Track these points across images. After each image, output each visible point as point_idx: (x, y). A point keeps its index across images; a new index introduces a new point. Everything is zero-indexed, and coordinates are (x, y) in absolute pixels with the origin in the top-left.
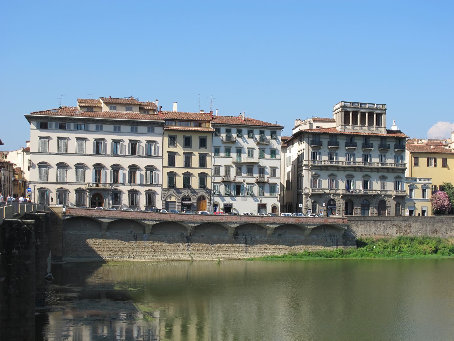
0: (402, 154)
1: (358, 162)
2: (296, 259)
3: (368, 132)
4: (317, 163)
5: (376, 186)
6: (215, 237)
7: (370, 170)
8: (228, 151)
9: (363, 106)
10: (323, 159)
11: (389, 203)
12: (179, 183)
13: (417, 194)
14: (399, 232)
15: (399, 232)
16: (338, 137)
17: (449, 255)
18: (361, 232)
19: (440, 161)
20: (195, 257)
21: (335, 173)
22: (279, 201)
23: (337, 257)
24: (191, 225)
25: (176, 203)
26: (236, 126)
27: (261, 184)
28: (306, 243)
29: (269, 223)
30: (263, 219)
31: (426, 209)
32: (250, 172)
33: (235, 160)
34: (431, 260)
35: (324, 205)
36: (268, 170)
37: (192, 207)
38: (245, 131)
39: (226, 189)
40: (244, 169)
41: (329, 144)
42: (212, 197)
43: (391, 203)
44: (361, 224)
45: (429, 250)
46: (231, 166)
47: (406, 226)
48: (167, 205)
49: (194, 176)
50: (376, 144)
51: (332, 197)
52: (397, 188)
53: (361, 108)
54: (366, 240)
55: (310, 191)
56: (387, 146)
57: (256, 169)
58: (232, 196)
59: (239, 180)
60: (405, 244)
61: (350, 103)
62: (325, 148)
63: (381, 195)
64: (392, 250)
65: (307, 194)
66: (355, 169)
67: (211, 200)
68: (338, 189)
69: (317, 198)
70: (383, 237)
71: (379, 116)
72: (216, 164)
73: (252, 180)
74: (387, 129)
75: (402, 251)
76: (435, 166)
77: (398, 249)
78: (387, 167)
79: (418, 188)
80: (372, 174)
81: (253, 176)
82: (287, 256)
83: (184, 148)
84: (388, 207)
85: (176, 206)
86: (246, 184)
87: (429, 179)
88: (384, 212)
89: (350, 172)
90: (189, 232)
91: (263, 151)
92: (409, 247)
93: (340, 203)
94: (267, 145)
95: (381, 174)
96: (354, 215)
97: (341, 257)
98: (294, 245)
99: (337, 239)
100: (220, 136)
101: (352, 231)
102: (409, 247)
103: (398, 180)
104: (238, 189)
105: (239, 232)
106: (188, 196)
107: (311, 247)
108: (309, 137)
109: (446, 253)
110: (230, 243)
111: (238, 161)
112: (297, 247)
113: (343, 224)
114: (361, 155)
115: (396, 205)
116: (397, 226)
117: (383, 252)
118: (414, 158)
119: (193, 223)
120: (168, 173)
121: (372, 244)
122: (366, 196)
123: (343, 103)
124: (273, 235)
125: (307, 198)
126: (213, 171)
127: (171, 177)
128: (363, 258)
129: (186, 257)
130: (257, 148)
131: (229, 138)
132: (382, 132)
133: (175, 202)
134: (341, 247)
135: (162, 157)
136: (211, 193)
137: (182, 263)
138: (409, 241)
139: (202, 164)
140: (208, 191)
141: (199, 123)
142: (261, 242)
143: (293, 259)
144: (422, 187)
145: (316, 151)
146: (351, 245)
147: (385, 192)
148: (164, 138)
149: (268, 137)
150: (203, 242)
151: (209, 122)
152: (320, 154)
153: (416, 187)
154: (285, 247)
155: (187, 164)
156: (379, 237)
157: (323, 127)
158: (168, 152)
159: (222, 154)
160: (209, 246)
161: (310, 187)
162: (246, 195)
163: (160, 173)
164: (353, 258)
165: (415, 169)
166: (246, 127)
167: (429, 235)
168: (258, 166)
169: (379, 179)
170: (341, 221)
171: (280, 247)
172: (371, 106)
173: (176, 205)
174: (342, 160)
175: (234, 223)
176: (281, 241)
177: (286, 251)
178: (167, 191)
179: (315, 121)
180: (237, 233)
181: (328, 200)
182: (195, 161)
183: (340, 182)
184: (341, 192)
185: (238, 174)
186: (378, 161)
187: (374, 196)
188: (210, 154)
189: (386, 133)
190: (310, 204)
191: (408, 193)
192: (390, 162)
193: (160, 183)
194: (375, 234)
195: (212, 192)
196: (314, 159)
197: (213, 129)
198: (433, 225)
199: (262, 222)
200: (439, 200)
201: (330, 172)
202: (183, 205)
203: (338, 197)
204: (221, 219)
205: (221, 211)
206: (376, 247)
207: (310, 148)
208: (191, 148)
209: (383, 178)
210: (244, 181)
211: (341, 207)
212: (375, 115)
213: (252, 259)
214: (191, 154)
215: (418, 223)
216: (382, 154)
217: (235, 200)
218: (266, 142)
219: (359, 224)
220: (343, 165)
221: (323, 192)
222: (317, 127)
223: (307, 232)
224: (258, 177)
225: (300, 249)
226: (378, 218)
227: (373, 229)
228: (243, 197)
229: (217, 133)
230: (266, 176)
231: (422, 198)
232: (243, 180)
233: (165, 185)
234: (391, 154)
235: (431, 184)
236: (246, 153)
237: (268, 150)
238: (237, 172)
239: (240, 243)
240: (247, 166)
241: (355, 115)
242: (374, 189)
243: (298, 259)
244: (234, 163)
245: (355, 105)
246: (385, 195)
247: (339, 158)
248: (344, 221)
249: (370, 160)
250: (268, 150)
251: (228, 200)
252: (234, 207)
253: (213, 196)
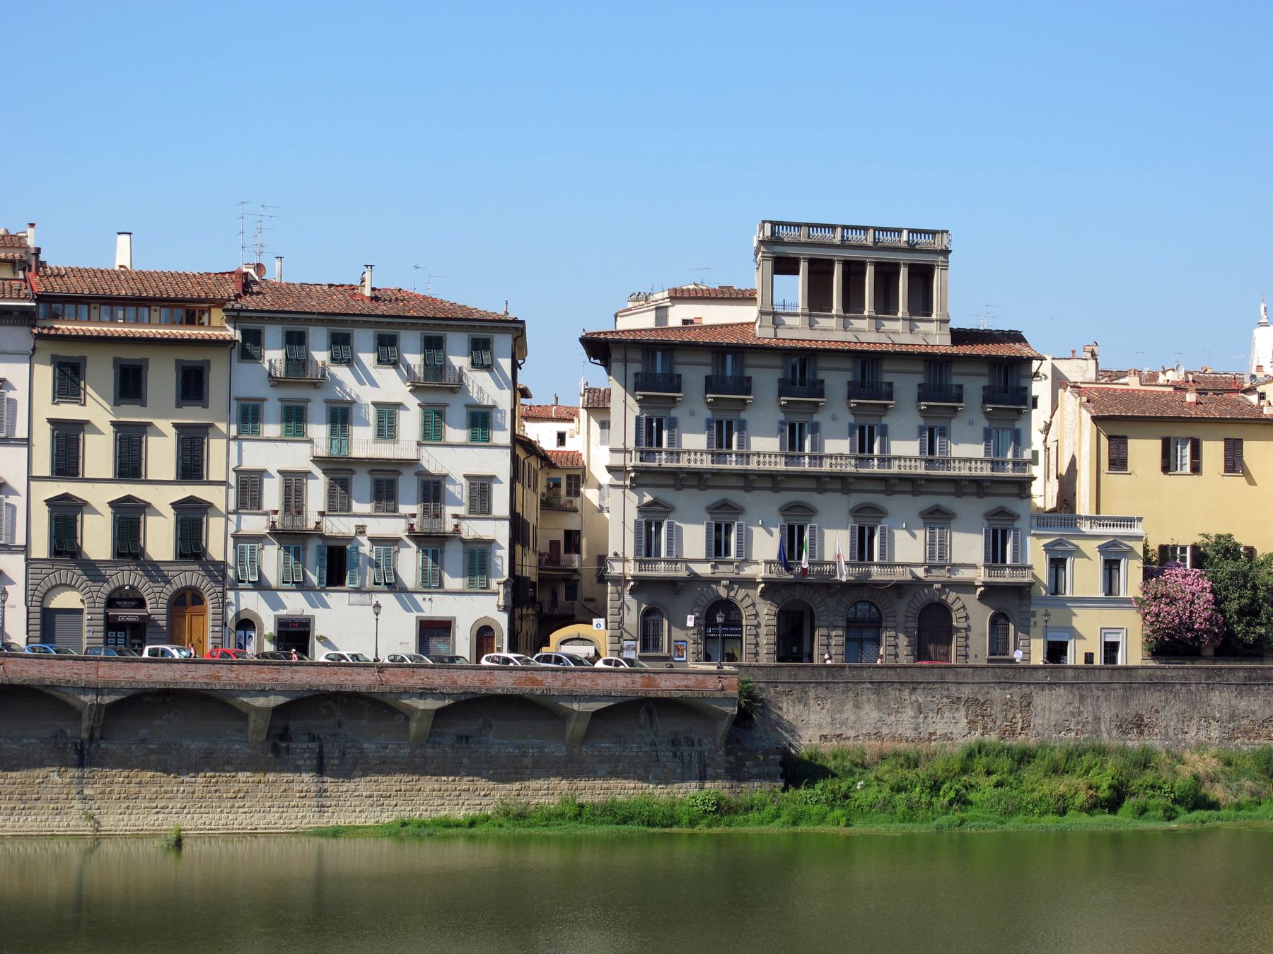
0: (1018, 425)
1: (831, 456)
2: (523, 831)
3: (872, 337)
4: (662, 461)
5: (908, 548)
6: (195, 746)
8: (295, 418)
9: (854, 237)
10: (685, 446)
11: (962, 613)
12: (97, 538)
13: (1084, 576)
14: (980, 725)
15: (980, 725)
17: (1170, 819)
18: (820, 726)
19: (1213, 451)
20: (111, 821)
21: (737, 497)
22: (505, 609)
23: (692, 823)
24: (88, 699)
25: (86, 617)
26: (326, 318)
27: (432, 543)
28: (571, 768)
29: (408, 692)
30: (386, 676)
32: (385, 495)
33: (322, 451)
34: (1094, 837)
35: (690, 623)
36: (458, 489)
37: (148, 630)
38: (363, 339)
39: (286, 564)
40: (362, 483)
41: (711, 385)
42: (231, 595)
43: (974, 617)
44: (817, 698)
45: (1081, 798)
46: (307, 474)
47: (1008, 704)
48: (47, 623)
49: (158, 514)
50: (906, 384)
51: (723, 592)
52: (995, 555)
53: (877, 246)
54: (835, 757)
55: (631, 570)
56: (885, 388)
57: (408, 485)
58: (311, 589)
59: (339, 526)
60: (989, 773)
61: (799, 225)
62: (694, 400)
63: (930, 584)
65: (620, 581)
66: (822, 482)
67: (225, 605)
68: (747, 561)
69: (660, 596)
70: (902, 746)
71: (922, 277)
72: (247, 465)
73: (392, 527)
74: (955, 324)
75: (970, 803)
76: (1196, 469)
77: (952, 794)
78: (952, 473)
79: (1084, 556)
80: (891, 503)
81: (395, 510)
82: (487, 818)
83: (116, 403)
84: (958, 630)
85: (85, 629)
86: (368, 544)
87: (1131, 520)
88: (942, 649)
89: (797, 496)
90: (86, 724)
91: (440, 414)
92: (999, 785)
93: (761, 618)
94: (453, 390)
95: (927, 502)
96: (816, 663)
97: (709, 825)
98: (522, 780)
99: (700, 754)
100: (261, 357)
101: (779, 722)
102: (999, 785)
103: (999, 525)
104: (337, 564)
105: (294, 725)
106: (132, 588)
108: (626, 361)
109: (1156, 808)
110: (255, 771)
111: (335, 453)
112: (534, 784)
113: (719, 695)
115: (993, 622)
116: (972, 702)
117: (887, 805)
118: (1110, 438)
119: (98, 691)
120: (49, 502)
121: (851, 773)
122: (860, 586)
123: (768, 226)
124: (433, 736)
125: (621, 595)
126: (233, 493)
127: (66, 517)
128: (802, 828)
129: (72, 820)
130: (413, 402)
131: (298, 365)
132: (932, 336)
133: (80, 611)
134: (719, 783)
135: (27, 442)
136: (225, 576)
137: (54, 846)
138: (1005, 763)
139: (191, 466)
140: (217, 570)
141: (191, 310)
142: (385, 767)
143: (509, 830)
144: (1102, 549)
145: (656, 414)
146: (760, 777)
147: (943, 572)
148: (37, 367)
149: (460, 361)
150: (145, 766)
151: (220, 303)
152: (673, 424)
154: (482, 783)
155: (129, 464)
156: (888, 746)
158: (51, 421)
159: (272, 429)
160: (170, 782)
161: (630, 553)
162: (369, 584)
163: (19, 502)
164: (763, 829)
165: (1113, 481)
166: (366, 325)
167: (1109, 737)
168: (418, 474)
169: (921, 522)
170: (712, 683)
171: (464, 783)
172: (887, 239)
173: (85, 623)
174: (765, 447)
175: (263, 692)
176: (465, 761)
177: (485, 801)
178: (47, 568)
179: (679, 296)
180: (286, 729)
182: (161, 454)
183: (758, 533)
184: (758, 572)
185: (338, 503)
186: (981, 454)
188: (222, 426)
190: (632, 619)
191: (1041, 570)
192: (967, 453)
193: (20, 540)
194: (878, 735)
195: (231, 573)
196: (650, 444)
197: (232, 333)
198: (1125, 699)
199: (382, 689)
200: (1173, 601)
201: (714, 496)
202: (111, 625)
203: (750, 592)
204: (210, 677)
205: (269, 647)
206: (863, 787)
207: (631, 401)
208: (144, 405)
209: (937, 518)
210: (361, 530)
211: (763, 631)
212: (905, 272)
213: (336, 833)
214: (144, 428)
215: (1061, 691)
216: (932, 424)
217: (326, 606)
218: (449, 379)
219: (812, 694)
220: (767, 467)
221: (909, 577)
222: (685, 322)
223: (575, 728)
224: (414, 516)
225: (545, 793)
226: (891, 672)
227: (870, 715)
228: (357, 591)
229: (250, 347)
230: (449, 510)
232: (358, 527)
233: (41, 548)
234: (971, 423)
235: (1139, 538)
236: (367, 424)
237: (457, 411)
238: (331, 495)
239: (298, 770)
240: (371, 472)
241: (853, 272)
242: (898, 559)
243: (531, 830)
244: (317, 460)
245: (818, 235)
247: (684, 436)
248: (725, 682)
249: (884, 448)
250: (457, 411)
251: (295, 604)
252: (319, 629)
253: (234, 588)
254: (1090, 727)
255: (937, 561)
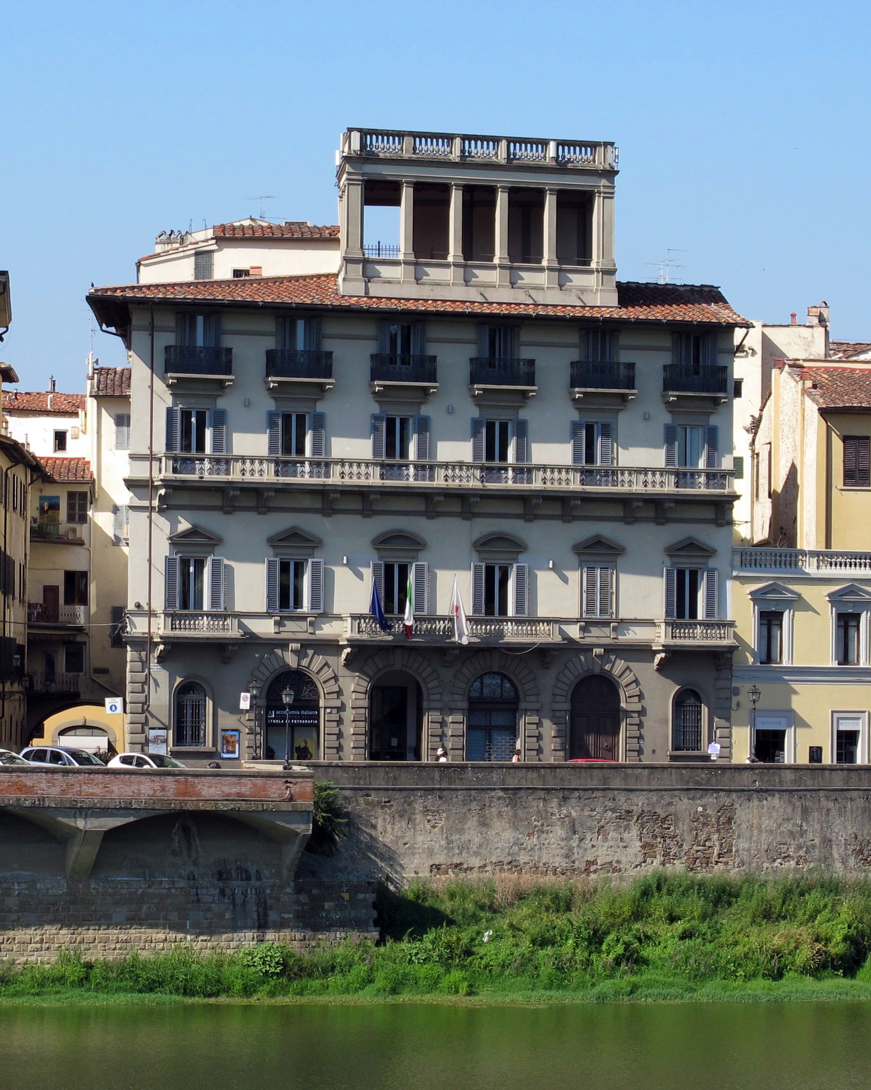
0: (714, 421)
1: (446, 465)
4: (204, 472)
5: (556, 597)
7: (518, 509)
9: (479, 151)
11: (634, 690)
13: (809, 637)
14: (659, 850)
15: (659, 850)
16: (230, 323)
18: (431, 852)
21: (312, 523)
23: (248, 991)
28: (74, 912)
31: (860, 725)
34: (822, 1011)
35: (245, 704)
41: (275, 363)
43: (652, 696)
44: (426, 811)
45: (804, 954)
47: (700, 821)
50: (554, 363)
51: (291, 660)
52: (681, 607)
53: (512, 165)
54: (452, 896)
56: (623, 372)
60: (672, 919)
61: (401, 135)
63: (588, 649)
64: (581, 955)
65: (144, 643)
68: (326, 616)
69: (201, 665)
70: (548, 880)
71: (577, 208)
74: (624, 276)
75: (646, 962)
77: (620, 949)
78: (626, 489)
79: (807, 607)
84: (628, 714)
88: (605, 742)
92: (686, 935)
93: (345, 697)
95: (583, 530)
96: (424, 761)
97: (272, 994)
99: (259, 891)
101: (372, 846)
102: (686, 935)
103: (687, 564)
107: (101, 933)
108: (152, 329)
112: (21, 934)
113: (286, 807)
114: (468, 428)
115: (679, 703)
117: (526, 965)
118: (845, 439)
121: (475, 918)
122: (487, 652)
123: (356, 137)
125: (145, 663)
128: (404, 997)
132: (591, 293)
134: (286, 934)
144: (834, 598)
145: (196, 405)
146: (345, 924)
147: (607, 631)
152: (220, 420)
153: (798, 603)
156: (528, 880)
157: (266, 273)
161: (159, 604)
164: (349, 999)
169: (575, 560)
170: (276, 790)
174: (352, 451)
179: (228, 237)
181: (266, 674)
183: (342, 576)
186: (661, 463)
187: (543, 654)
189: (613, 299)
191: (747, 628)
192: (641, 461)
194: (513, 865)
203: (331, 660)
206: (492, 939)
207: (159, 385)
209: (598, 554)
211: (349, 715)
212: (554, 201)
215: (775, 801)
216: (590, 419)
219: (418, 806)
220: (355, 481)
221: (558, 639)
222: (237, 273)
223: (80, 854)
226: (532, 775)
227: (502, 835)
231: (834, 664)
242: (542, 613)
243: (18, 1001)
246: (610, 650)
248: (295, 789)
254: (816, 854)
255: (598, 616)
